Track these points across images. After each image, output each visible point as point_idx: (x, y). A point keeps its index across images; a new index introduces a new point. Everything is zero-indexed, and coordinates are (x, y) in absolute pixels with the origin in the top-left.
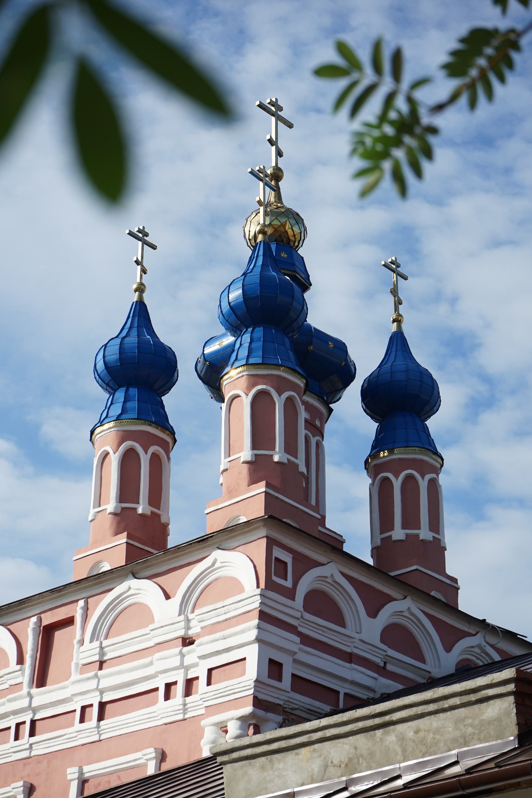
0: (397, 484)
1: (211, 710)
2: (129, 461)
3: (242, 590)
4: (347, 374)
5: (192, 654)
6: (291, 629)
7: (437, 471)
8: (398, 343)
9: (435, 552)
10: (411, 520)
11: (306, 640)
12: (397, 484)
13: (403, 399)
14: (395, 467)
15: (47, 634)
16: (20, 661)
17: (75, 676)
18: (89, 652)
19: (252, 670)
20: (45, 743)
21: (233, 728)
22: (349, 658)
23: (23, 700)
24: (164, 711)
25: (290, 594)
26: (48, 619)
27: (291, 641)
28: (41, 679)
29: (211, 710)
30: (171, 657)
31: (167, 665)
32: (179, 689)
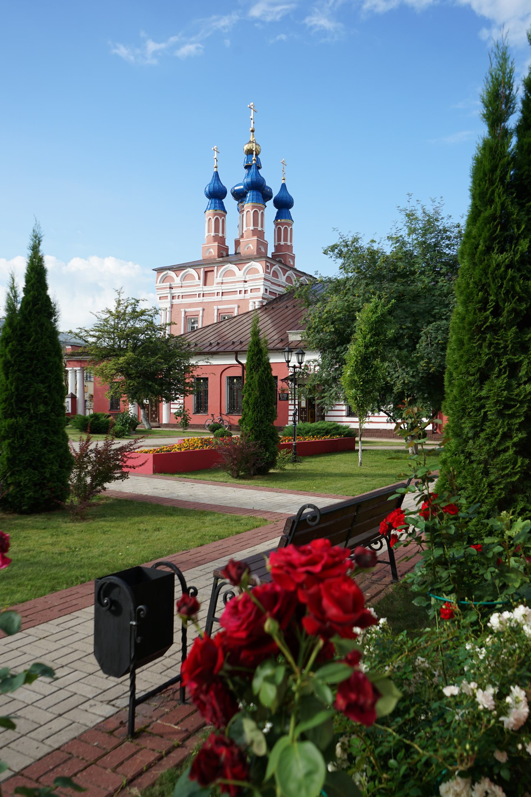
0: (283, 229)
1: (251, 298)
2: (217, 220)
3: (259, 272)
4: (275, 201)
5: (247, 285)
6: (269, 281)
7: (290, 225)
8: (284, 186)
9: (290, 248)
10: (286, 240)
11: (272, 283)
12: (283, 229)
13: (284, 205)
14: (282, 224)
15: (206, 273)
16: (199, 279)
17: (215, 285)
18: (219, 280)
19: (262, 291)
20: (207, 299)
21: (257, 303)
22: (279, 286)
23: (201, 289)
24: (238, 296)
25: (269, 273)
26: (206, 270)
27: (269, 284)
28: (205, 284)
29: (251, 298)
30: (242, 284)
31: (240, 286)
32: (243, 292)
